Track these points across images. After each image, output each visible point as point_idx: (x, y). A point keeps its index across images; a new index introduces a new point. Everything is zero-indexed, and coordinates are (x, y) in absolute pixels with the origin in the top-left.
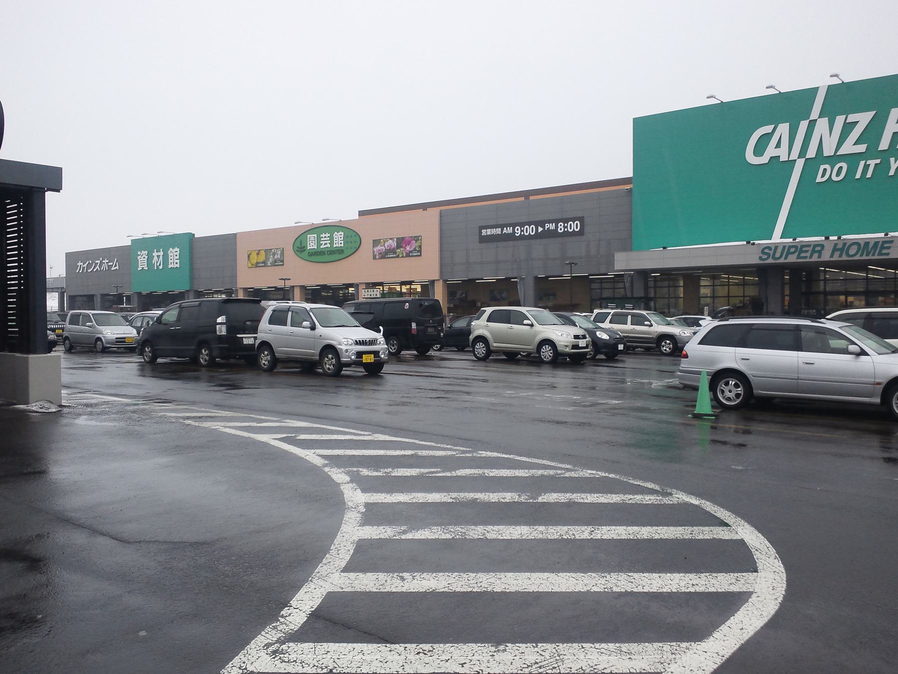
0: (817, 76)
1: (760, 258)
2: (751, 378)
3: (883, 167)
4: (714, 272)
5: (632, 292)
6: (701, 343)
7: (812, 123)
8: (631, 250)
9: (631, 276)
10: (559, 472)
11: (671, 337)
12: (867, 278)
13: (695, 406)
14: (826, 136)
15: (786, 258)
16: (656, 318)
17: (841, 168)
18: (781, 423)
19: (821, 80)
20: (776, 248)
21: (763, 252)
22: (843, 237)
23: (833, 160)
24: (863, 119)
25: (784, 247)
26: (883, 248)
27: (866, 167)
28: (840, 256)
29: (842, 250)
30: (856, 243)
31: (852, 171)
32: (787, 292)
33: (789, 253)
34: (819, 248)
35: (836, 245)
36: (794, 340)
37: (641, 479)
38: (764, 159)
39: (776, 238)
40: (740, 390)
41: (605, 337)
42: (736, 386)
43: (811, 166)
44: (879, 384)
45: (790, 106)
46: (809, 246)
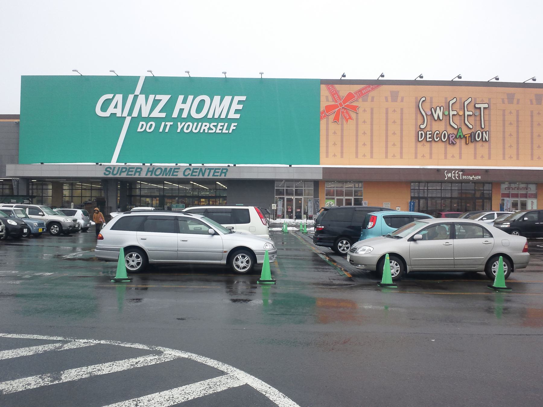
0: (140, 69)
1: (105, 174)
2: (148, 253)
3: (174, 127)
4: (72, 181)
5: (18, 192)
6: (112, 228)
7: (136, 97)
8: (18, 163)
9: (18, 181)
10: (57, 345)
11: (58, 223)
12: (164, 188)
13: (115, 272)
14: (144, 106)
15: (120, 175)
16: (46, 210)
17: (151, 125)
18: (172, 281)
19: (143, 74)
20: (114, 168)
21: (106, 170)
22: (153, 164)
23: (148, 119)
24: (165, 98)
25: (119, 168)
26: (174, 172)
27: (166, 126)
28: (151, 175)
29: (152, 172)
30: (160, 168)
31: (157, 127)
32: (119, 195)
33: (122, 172)
34: (139, 170)
35: (149, 168)
36: (175, 226)
37: (128, 341)
38: (107, 114)
39: (114, 162)
40: (140, 260)
41: (14, 223)
42: (137, 257)
43: (135, 121)
44: (225, 252)
45: (123, 85)
46: (134, 168)
